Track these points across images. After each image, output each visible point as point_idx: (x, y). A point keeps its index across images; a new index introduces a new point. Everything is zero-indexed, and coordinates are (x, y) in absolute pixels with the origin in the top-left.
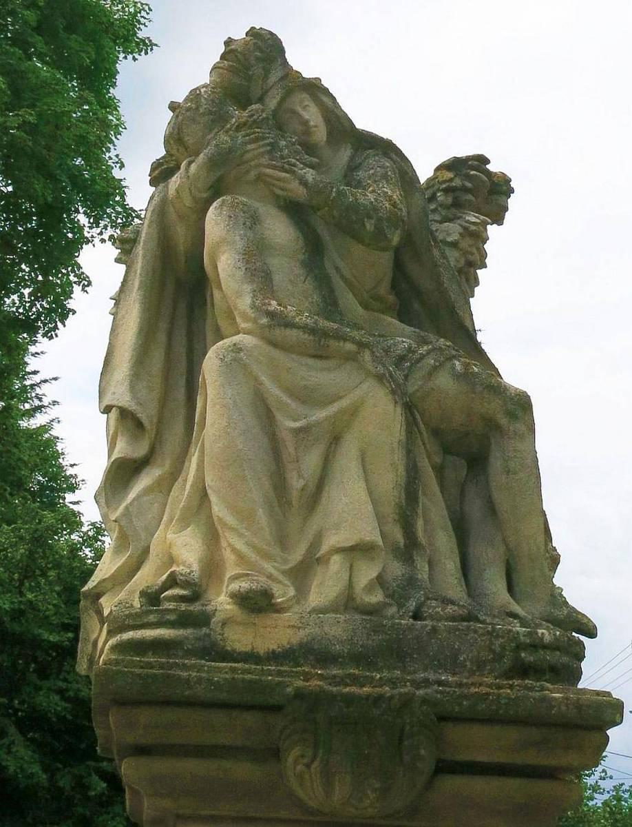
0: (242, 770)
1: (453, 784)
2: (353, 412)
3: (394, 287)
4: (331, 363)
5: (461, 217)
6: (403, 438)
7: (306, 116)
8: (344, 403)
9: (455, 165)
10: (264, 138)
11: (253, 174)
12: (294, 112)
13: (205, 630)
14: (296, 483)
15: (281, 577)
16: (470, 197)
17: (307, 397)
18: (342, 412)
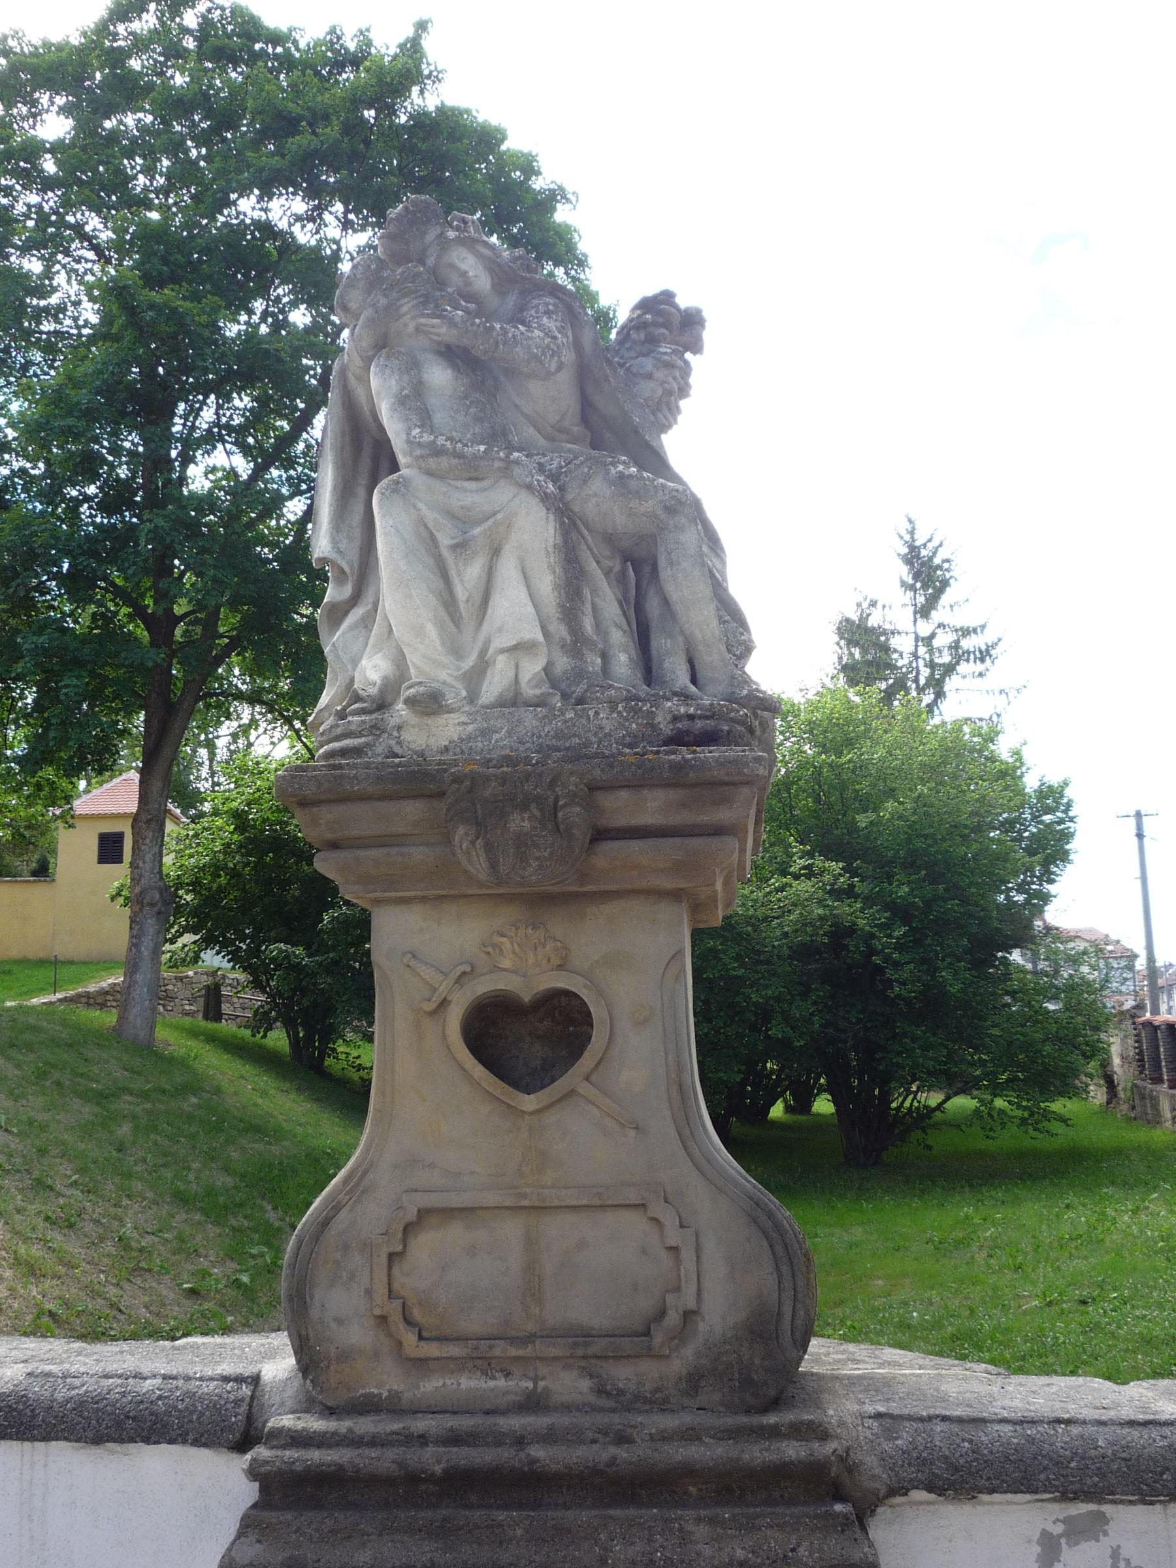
1: (609, 847)
3: (585, 420)
5: (653, 351)
6: (559, 541)
7: (463, 267)
9: (646, 305)
11: (411, 326)
12: (453, 267)
13: (1138, 1082)
14: (461, 594)
16: (663, 331)
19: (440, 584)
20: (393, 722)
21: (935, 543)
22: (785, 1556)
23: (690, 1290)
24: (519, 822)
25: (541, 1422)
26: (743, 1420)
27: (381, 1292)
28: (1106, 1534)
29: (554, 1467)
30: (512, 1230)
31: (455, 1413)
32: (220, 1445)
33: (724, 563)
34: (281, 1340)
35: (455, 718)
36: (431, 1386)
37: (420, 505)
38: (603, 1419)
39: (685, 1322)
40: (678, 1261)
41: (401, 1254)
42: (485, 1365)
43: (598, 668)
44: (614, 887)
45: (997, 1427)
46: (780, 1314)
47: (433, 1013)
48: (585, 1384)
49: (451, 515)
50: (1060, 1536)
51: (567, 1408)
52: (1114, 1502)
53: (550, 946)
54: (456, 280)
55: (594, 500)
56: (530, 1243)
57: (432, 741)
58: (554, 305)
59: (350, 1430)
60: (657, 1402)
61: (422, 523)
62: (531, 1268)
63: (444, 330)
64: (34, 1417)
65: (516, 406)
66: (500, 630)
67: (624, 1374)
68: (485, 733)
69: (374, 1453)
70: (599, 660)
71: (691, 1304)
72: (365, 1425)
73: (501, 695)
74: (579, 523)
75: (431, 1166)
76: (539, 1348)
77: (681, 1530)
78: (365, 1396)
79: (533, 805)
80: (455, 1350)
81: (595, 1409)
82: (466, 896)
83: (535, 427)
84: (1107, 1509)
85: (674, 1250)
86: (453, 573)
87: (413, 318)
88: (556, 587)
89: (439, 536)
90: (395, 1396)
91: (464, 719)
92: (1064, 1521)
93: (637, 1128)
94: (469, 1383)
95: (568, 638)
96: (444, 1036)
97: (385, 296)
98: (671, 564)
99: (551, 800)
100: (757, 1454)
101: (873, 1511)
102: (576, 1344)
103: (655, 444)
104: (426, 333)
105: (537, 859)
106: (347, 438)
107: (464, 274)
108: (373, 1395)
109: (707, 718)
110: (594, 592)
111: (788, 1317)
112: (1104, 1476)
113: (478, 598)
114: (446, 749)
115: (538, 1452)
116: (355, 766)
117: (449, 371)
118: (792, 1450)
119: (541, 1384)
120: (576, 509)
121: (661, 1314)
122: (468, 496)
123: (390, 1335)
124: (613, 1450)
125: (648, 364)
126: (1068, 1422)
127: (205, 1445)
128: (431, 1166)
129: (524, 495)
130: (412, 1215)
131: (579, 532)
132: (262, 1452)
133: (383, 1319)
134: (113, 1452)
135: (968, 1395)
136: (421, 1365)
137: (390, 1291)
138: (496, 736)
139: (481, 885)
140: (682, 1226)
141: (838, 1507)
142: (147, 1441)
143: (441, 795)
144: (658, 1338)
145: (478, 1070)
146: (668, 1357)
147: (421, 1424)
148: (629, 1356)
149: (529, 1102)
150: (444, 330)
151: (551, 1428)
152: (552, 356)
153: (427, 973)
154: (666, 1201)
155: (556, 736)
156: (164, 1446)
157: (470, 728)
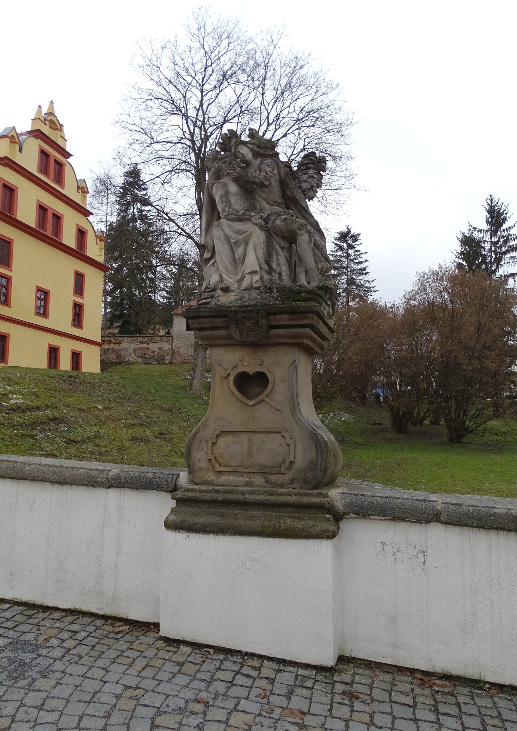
0: (222, 332)
2: (250, 235)
4: (244, 223)
6: (265, 240)
7: (242, 152)
8: (247, 233)
10: (226, 162)
11: (226, 172)
12: (239, 152)
15: (234, 283)
16: (311, 165)
17: (239, 232)
18: (247, 236)
19: (232, 254)
20: (216, 295)
25: (249, 489)
26: (305, 491)
27: (210, 452)
29: (251, 500)
30: (245, 437)
33: (325, 243)
36: (223, 479)
39: (290, 465)
40: (289, 448)
41: (215, 443)
42: (235, 473)
43: (277, 278)
54: (241, 156)
56: (250, 441)
57: (227, 300)
58: (271, 163)
59: (200, 488)
62: (249, 448)
64: (121, 481)
66: (247, 267)
67: (273, 478)
68: (241, 298)
71: (292, 460)
72: (204, 488)
73: (246, 287)
74: (272, 233)
75: (224, 419)
78: (205, 480)
85: (288, 445)
88: (264, 254)
90: (213, 480)
91: (236, 294)
94: (232, 478)
96: (228, 384)
102: (261, 469)
103: (304, 205)
105: (253, 334)
108: (207, 480)
110: (277, 254)
112: (406, 514)
113: (242, 258)
114: (231, 303)
115: (247, 496)
116: (204, 308)
123: (212, 465)
124: (268, 497)
126: (398, 498)
128: (224, 419)
129: (255, 226)
130: (218, 433)
133: (210, 460)
135: (470, 508)
138: (245, 299)
141: (327, 516)
144: (283, 468)
145: (237, 393)
147: (217, 488)
149: (251, 403)
151: (252, 490)
157: (238, 297)
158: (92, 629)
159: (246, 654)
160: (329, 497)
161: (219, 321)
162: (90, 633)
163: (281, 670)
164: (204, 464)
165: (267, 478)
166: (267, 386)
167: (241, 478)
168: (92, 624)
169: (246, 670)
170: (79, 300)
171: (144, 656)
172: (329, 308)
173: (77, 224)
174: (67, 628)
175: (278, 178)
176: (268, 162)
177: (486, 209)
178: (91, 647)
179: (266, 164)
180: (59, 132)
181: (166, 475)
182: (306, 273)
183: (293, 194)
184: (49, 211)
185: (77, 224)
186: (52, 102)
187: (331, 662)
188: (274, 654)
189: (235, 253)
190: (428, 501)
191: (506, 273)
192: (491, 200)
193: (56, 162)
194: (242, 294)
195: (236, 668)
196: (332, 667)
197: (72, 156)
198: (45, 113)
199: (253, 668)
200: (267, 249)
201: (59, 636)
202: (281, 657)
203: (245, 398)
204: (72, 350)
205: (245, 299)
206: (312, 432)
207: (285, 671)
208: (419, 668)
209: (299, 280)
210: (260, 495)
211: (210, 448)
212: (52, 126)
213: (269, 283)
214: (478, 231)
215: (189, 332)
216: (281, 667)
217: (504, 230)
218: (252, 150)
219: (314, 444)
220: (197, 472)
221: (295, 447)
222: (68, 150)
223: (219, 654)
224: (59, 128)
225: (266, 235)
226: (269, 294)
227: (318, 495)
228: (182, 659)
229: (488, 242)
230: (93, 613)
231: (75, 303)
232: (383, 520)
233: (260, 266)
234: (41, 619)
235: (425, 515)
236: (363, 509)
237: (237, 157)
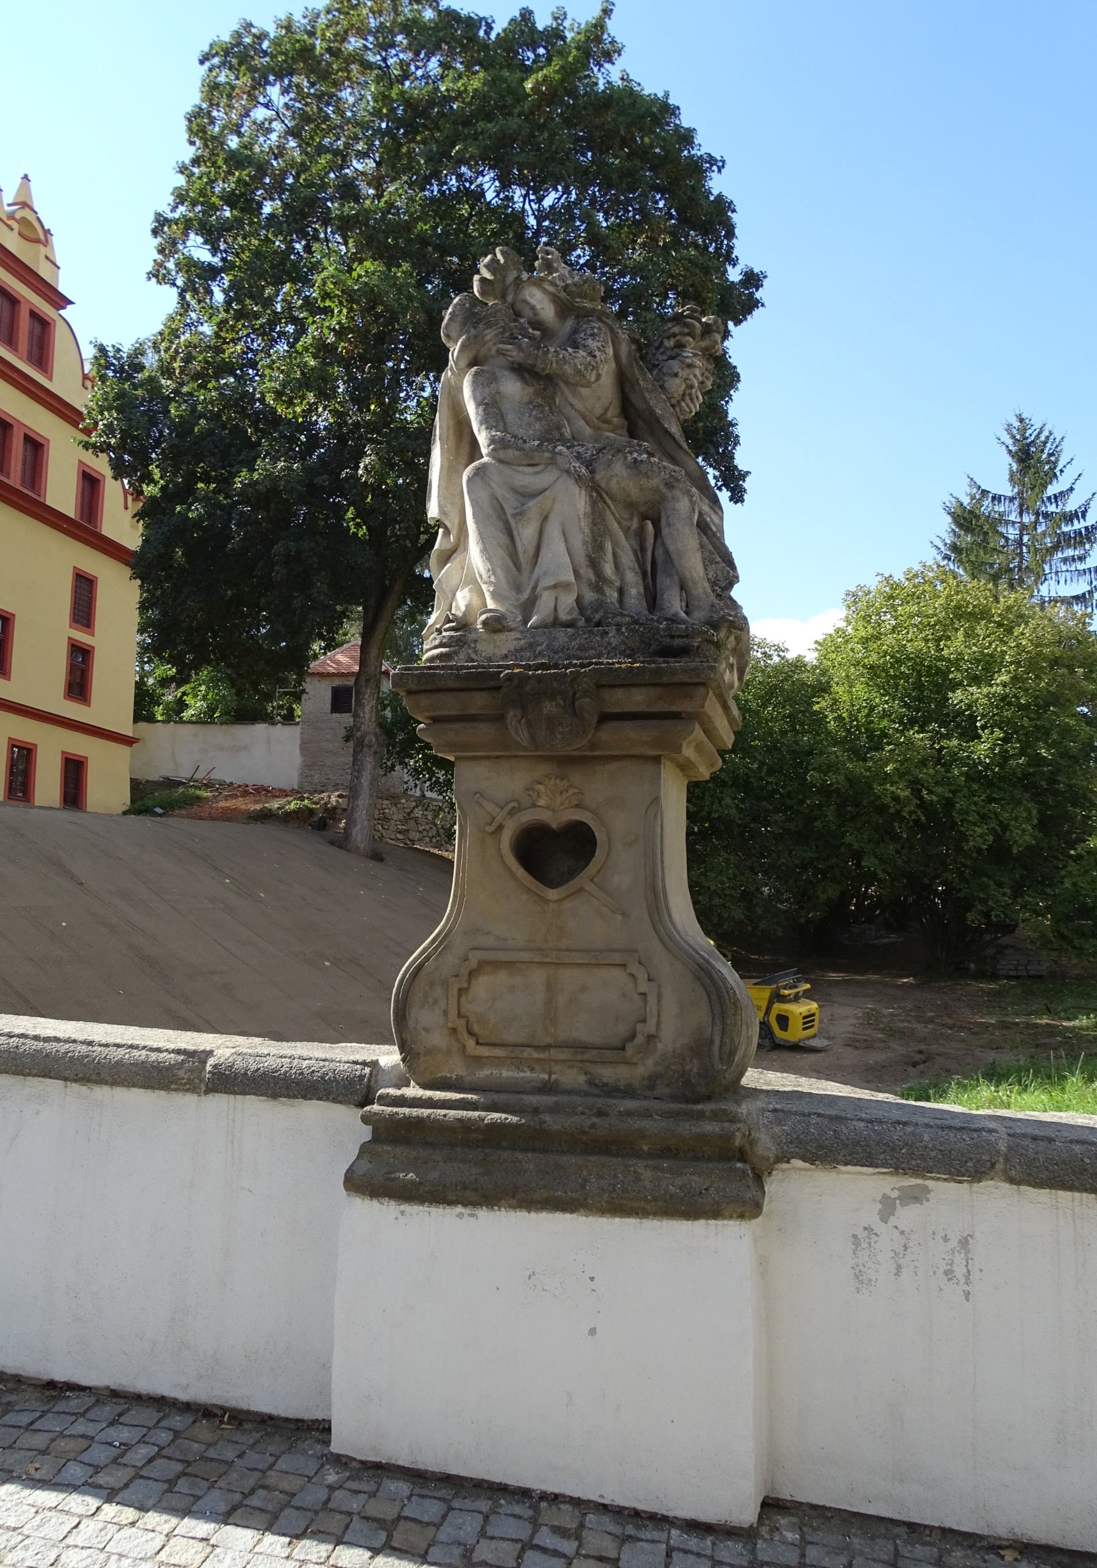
6: (588, 509)
7: (533, 301)
11: (494, 349)
19: (507, 541)
21: (1046, 433)
22: (701, 1193)
23: (652, 1022)
24: (549, 707)
27: (453, 1013)
28: (928, 1200)
30: (538, 977)
31: (498, 1092)
32: (350, 1103)
33: (722, 519)
34: (396, 1048)
35: (513, 635)
37: (493, 485)
38: (590, 1100)
40: (646, 1002)
41: (467, 989)
42: (518, 1063)
44: (615, 753)
45: (855, 1123)
46: (712, 1041)
47: (493, 833)
48: (582, 1078)
49: (515, 491)
50: (895, 1199)
51: (570, 1092)
52: (932, 1178)
53: (571, 791)
54: (527, 312)
55: (615, 479)
56: (549, 986)
57: (497, 651)
58: (599, 329)
60: (628, 1092)
61: (494, 498)
62: (549, 1002)
63: (515, 353)
65: (571, 405)
66: (545, 573)
67: (607, 1074)
68: (531, 646)
69: (443, 1112)
70: (616, 595)
74: (605, 496)
75: (488, 933)
76: (554, 1053)
77: (635, 1172)
78: (442, 1077)
79: (559, 697)
80: (499, 1052)
81: (587, 1094)
82: (516, 756)
83: (584, 419)
84: (930, 1184)
85: (643, 995)
86: (515, 533)
87: (495, 344)
88: (585, 543)
89: (506, 507)
90: (460, 1078)
91: (518, 635)
92: (900, 1189)
93: (623, 914)
95: (593, 578)
96: (499, 850)
97: (475, 328)
98: (669, 525)
99: (571, 694)
100: (686, 1129)
101: (770, 1174)
104: (504, 355)
105: (561, 733)
106: (451, 431)
107: (533, 308)
109: (683, 637)
110: (615, 545)
111: (717, 1042)
117: (518, 384)
118: (711, 1128)
119: (554, 1077)
120: (603, 485)
121: (633, 1036)
122: (527, 478)
123: (458, 1040)
125: (675, 365)
127: (340, 1102)
128: (488, 933)
130: (473, 963)
131: (605, 502)
132: (376, 1108)
133: (454, 1030)
134: (284, 1104)
136: (478, 1061)
137: (459, 1012)
138: (539, 648)
139: (525, 749)
140: (649, 980)
141: (739, 1165)
142: (305, 1097)
143: (498, 688)
144: (630, 1050)
145: (520, 872)
146: (636, 1064)
148: (610, 1062)
149: (553, 894)
150: (515, 353)
151: (556, 1103)
152: (592, 370)
153: (489, 807)
154: (640, 963)
155: (579, 649)
156: (315, 1102)
157: (522, 642)
158: (164, 1437)
159: (544, 1496)
160: (739, 1121)
161: (479, 702)
162: (161, 1448)
163: (630, 1537)
164: (438, 1039)
165: (590, 1074)
166: (592, 853)
167: (528, 1074)
168: (164, 1424)
169: (545, 1538)
170: (82, 637)
171: (299, 1504)
172: (731, 671)
173: (80, 462)
174: (102, 1437)
175: (613, 365)
176: (593, 328)
177: (1010, 451)
178: (166, 1486)
179: (589, 332)
180: (41, 246)
181: (346, 1066)
182: (683, 587)
183: (647, 403)
184: (15, 429)
185: (80, 462)
186: (26, 177)
187: (747, 1515)
188: (610, 1498)
189: (517, 538)
190: (975, 1130)
191: (1053, 594)
192: (1023, 431)
193: (34, 315)
194: (533, 637)
195: (524, 1532)
196: (751, 1526)
197: (72, 303)
198: (11, 201)
199: (560, 1531)
200: (592, 531)
201: (85, 1457)
202: (627, 1505)
203: (534, 881)
204: (63, 752)
205: (539, 648)
206: (699, 965)
207: (641, 1540)
208: (955, 1527)
209: (667, 604)
210: (576, 1114)
211: (453, 1001)
212: (25, 232)
213: (597, 611)
214: (994, 498)
215: (338, 715)
216: (630, 1530)
217: (1049, 498)
218: (555, 299)
219: (704, 994)
220: (422, 1059)
221: (659, 1001)
222: (61, 289)
223: (478, 1497)
224: (42, 237)
225: (591, 496)
226: (598, 638)
227: (716, 1116)
228: (389, 1512)
229: (1014, 523)
230: (163, 1397)
231: (73, 645)
232: (867, 1175)
233: (576, 572)
234: (38, 1414)
235: (970, 1164)
236: (823, 1148)
237: (518, 314)
